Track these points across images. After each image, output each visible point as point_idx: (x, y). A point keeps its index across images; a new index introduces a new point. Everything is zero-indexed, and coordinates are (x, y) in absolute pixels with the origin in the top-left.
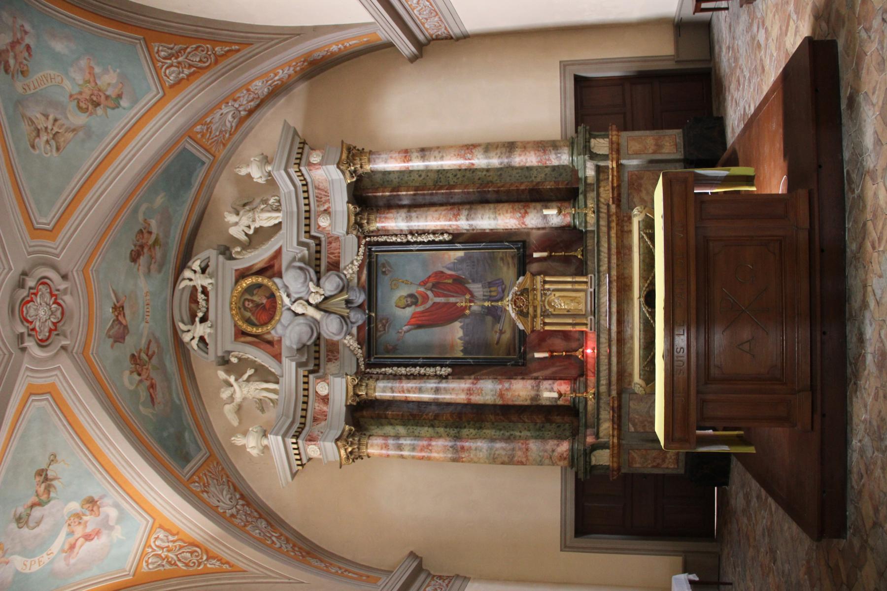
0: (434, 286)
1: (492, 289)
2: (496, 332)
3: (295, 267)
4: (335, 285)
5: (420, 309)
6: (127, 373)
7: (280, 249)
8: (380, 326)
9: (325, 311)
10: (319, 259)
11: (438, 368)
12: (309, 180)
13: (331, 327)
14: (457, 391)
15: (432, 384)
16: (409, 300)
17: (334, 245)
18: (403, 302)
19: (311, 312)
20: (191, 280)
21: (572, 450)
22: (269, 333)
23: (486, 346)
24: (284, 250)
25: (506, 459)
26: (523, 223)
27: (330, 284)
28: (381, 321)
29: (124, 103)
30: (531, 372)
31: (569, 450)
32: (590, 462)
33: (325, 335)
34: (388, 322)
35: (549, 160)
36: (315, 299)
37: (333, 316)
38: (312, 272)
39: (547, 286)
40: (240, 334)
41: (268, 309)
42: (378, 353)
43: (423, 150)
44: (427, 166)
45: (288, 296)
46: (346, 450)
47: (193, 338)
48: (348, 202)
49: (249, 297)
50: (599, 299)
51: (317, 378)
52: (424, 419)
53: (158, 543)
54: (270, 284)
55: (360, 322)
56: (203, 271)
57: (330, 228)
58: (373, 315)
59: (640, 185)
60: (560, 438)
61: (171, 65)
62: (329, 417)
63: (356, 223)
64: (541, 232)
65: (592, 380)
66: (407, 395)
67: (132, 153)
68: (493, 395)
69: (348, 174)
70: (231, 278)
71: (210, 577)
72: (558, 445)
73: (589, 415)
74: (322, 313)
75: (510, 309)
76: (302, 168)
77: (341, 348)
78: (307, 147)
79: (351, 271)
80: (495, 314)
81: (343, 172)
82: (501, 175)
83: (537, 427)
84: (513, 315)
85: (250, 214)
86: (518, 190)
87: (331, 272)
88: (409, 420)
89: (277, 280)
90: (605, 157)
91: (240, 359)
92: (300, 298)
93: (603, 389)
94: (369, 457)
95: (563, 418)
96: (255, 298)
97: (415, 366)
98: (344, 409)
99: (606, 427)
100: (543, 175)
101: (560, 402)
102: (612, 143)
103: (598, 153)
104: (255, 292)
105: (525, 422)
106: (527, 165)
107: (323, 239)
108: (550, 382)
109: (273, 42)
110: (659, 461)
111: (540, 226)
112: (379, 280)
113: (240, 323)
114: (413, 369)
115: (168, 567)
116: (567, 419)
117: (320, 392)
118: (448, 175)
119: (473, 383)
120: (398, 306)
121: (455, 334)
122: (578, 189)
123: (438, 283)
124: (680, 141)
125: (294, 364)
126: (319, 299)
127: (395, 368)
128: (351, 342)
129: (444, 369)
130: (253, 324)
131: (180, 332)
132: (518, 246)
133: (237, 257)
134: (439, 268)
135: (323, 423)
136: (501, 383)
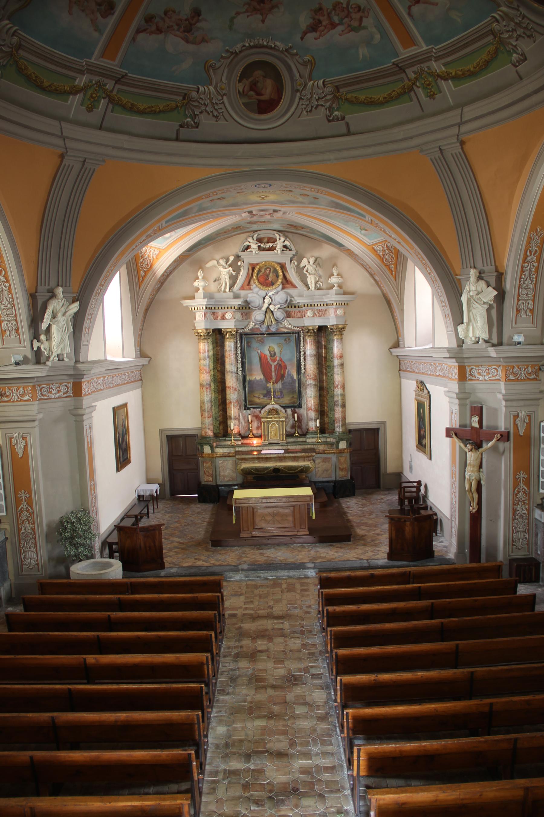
0: (280, 365)
3: (287, 297)
5: (269, 359)
9: (266, 312)
11: (241, 369)
13: (258, 316)
15: (234, 369)
17: (299, 314)
18: (271, 350)
19: (266, 306)
20: (280, 239)
23: (251, 391)
25: (203, 408)
27: (279, 314)
29: (363, 232)
34: (262, 342)
36: (272, 307)
37: (264, 317)
40: (253, 267)
41: (266, 283)
42: (245, 338)
49: (272, 271)
53: (152, 251)
54: (279, 283)
55: (261, 330)
56: (285, 246)
59: (325, 462)
61: (383, 248)
62: (216, 321)
63: (309, 330)
71: (136, 272)
80: (268, 394)
85: (314, 272)
89: (281, 287)
90: (337, 447)
91: (240, 266)
92: (272, 300)
95: (223, 431)
96: (271, 275)
97: (242, 358)
99: (219, 451)
102: (344, 450)
109: (396, 290)
110: (207, 473)
115: (140, 255)
116: (222, 431)
120: (268, 347)
121: (257, 376)
122: (325, 433)
124: (345, 478)
127: (240, 348)
130: (258, 274)
134: (289, 367)
135: (212, 318)
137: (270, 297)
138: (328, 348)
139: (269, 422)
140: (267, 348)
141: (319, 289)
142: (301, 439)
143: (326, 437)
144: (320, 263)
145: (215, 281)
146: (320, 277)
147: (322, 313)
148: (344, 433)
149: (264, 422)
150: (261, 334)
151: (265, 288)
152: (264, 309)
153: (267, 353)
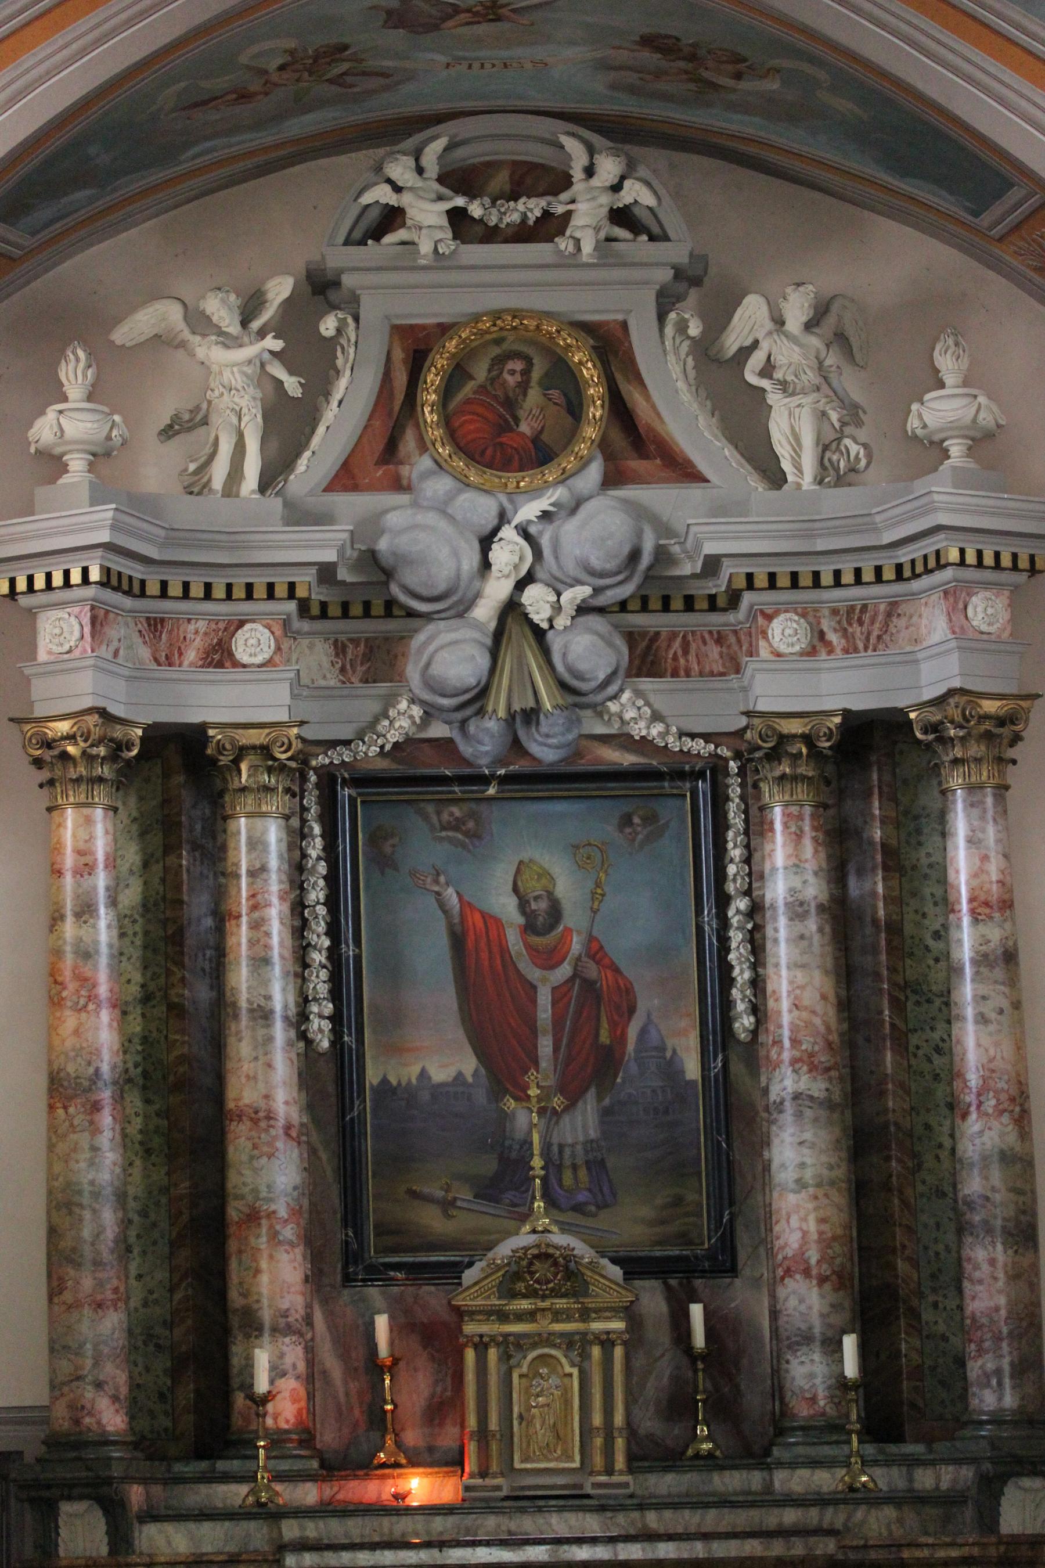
0: (589, 986)
1: (583, 1173)
2: (448, 1189)
3: (639, 534)
4: (582, 666)
5: (513, 940)
6: (292, 44)
7: (702, 479)
8: (456, 811)
9: (499, 634)
10: (666, 606)
11: (328, 1008)
12: (915, 585)
13: (451, 654)
14: (267, 1076)
15: (280, 996)
16: (543, 905)
17: (714, 651)
18: (532, 886)
19: (497, 590)
21: (105, 1441)
22: (423, 447)
24: (694, 493)
25: (66, 1243)
26: (788, 1272)
27: (587, 650)
28: (472, 815)
30: (325, 1302)
31: (104, 1432)
32: (69, 1498)
33: (421, 637)
34: (472, 836)
35: (981, 1352)
36: (537, 601)
37: (483, 661)
38: (627, 590)
39: (596, 1351)
40: (416, 346)
41: (502, 446)
42: (368, 805)
43: (1010, 957)
44: (959, 970)
45: (546, 516)
46: (71, 738)
47: (398, 189)
48: (847, 713)
49: (536, 375)
50: (561, 1509)
51: (286, 624)
52: (169, 973)
54: (583, 448)
55: (466, 749)
56: (622, 216)
57: (764, 653)
58: (492, 791)
60: (134, 1408)
63: (783, 739)
64: (766, 1324)
65: (309, 1494)
66: (244, 919)
67: (979, 75)
68: (255, 1191)
69: (935, 716)
70: (596, 306)
72: (115, 1399)
73: (204, 1489)
74: (493, 625)
75: (523, 1239)
76: (948, 573)
77: (383, 688)
78: (1022, 578)
79: (630, 714)
80: (505, 1181)
81: (939, 701)
82: (944, 1195)
83: (159, 1330)
84: (504, 1250)
85: (810, 377)
86: (894, 1251)
87: (625, 650)
88: (165, 923)
89: (595, 472)
90: (988, 1520)
91: (331, 343)
92: (538, 554)
93: (290, 1530)
94: (50, 810)
95: (196, 1407)
96: (534, 396)
97: (333, 931)
98: (195, 718)
100: (941, 1328)
101: (240, 1400)
103: (1004, 1501)
104: (555, 393)
105: (171, 1290)
106: (966, 1284)
107: (731, 617)
108: (301, 1366)
111: (782, 1321)
112: (608, 803)
113: (451, 346)
114: (322, 928)
116: (188, 1420)
117: (241, 635)
118: (941, 1026)
119: (288, 1128)
120: (524, 869)
121: (437, 1057)
122: (899, 1438)
123: (598, 998)
125: (330, 556)
126: (540, 615)
127: (322, 868)
128: (403, 720)
129: (327, 1025)
130: (447, 392)
131: (410, 143)
132: (706, 1244)
133: (669, 330)
134: (647, 1002)
135: (144, 653)
136: (295, 1212)
137: (524, 532)
138: (912, 863)
139: (511, 1347)
140: (502, 875)
141: (840, 481)
142: (730, 1481)
143: (912, 1462)
144: (851, 332)
145: (168, 432)
146: (853, 414)
147: (865, 629)
148: (1031, 1422)
149: (481, 1346)
150: (463, 780)
151: (491, 478)
152: (485, 611)
153: (505, 906)
